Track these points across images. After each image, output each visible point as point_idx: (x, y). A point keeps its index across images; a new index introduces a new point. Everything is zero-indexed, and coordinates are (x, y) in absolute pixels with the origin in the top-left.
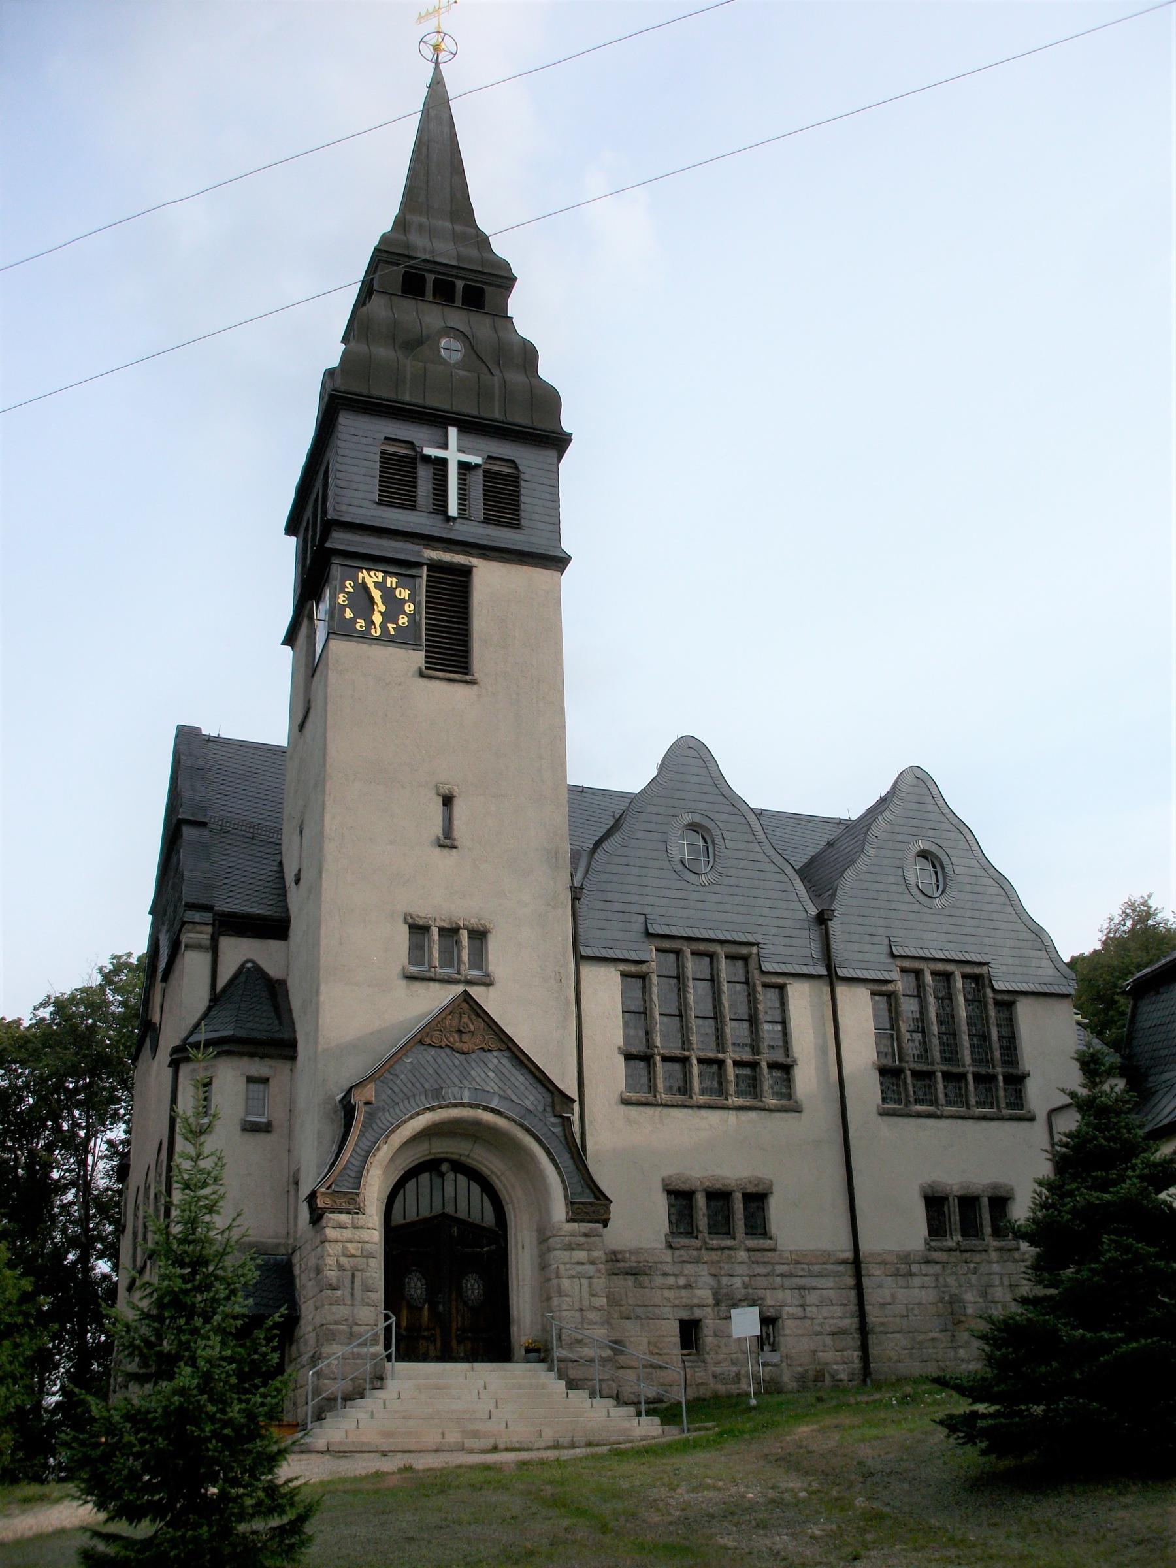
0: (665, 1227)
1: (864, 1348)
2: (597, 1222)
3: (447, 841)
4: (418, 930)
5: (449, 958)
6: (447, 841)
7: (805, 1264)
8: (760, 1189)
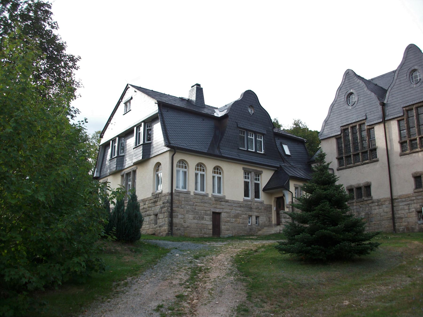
0: (414, 187)
1: (394, 223)
7: (380, 203)
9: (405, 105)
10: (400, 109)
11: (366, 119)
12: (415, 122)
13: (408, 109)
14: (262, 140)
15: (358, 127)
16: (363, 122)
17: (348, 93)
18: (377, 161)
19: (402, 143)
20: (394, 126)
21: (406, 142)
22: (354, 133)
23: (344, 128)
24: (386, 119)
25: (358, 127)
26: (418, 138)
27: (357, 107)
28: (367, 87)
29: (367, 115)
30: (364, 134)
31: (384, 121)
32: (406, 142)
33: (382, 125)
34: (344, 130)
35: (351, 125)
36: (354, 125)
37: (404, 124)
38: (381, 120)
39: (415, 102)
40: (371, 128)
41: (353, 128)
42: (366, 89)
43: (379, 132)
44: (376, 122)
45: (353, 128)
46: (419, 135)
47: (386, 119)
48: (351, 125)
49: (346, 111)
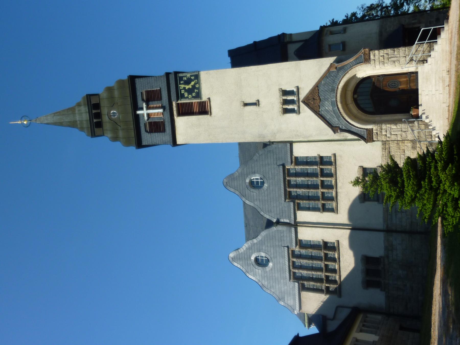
2: (370, 54)
3: (257, 104)
4: (286, 111)
5: (292, 102)
6: (257, 104)
7: (389, 248)
8: (361, 170)
9: (283, 199)
10: (286, 204)
11: (288, 247)
12: (304, 190)
13: (289, 197)
14: (432, 28)
15: (295, 260)
16: (290, 252)
17: (254, 263)
18: (338, 241)
19: (324, 209)
20: (303, 216)
21: (323, 193)
22: (301, 267)
23: (292, 277)
24: (293, 222)
25: (295, 260)
26: (322, 190)
27: (272, 256)
28: (254, 238)
29: (283, 245)
30: (303, 251)
31: (296, 225)
32: (323, 193)
33: (300, 229)
34: (296, 278)
35: (291, 267)
36: (291, 264)
37: (303, 203)
38: (293, 229)
39: (282, 186)
40: (302, 244)
41: (294, 266)
42: (255, 241)
43: (306, 234)
44: (293, 235)
45: (295, 266)
46: (318, 188)
47: (293, 222)
48: (291, 267)
49: (273, 271)
